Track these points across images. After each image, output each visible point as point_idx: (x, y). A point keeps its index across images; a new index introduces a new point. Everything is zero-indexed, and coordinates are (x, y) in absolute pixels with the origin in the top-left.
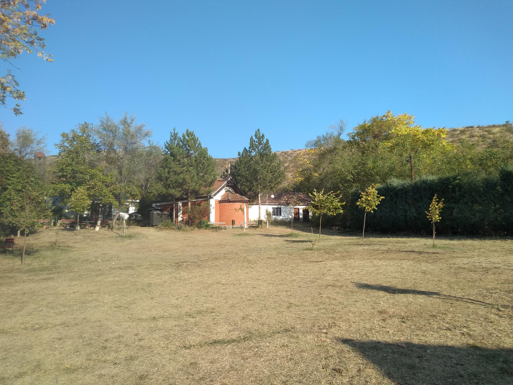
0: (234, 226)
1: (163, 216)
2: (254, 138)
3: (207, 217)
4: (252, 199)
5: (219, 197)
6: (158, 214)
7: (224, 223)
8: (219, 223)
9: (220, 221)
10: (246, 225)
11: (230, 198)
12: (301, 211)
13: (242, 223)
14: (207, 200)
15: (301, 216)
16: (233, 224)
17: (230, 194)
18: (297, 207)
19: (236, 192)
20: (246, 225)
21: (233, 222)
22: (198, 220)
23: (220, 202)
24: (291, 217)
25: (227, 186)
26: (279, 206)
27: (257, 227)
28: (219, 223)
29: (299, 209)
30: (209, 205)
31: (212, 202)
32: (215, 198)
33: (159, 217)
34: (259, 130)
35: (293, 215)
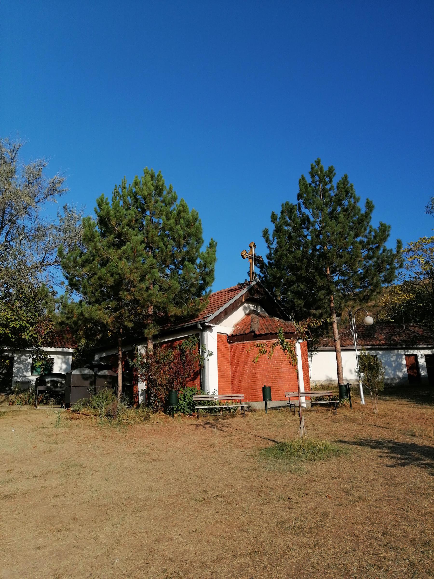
0: (270, 404)
1: (99, 381)
2: (309, 180)
3: (198, 381)
4: (318, 340)
5: (228, 326)
6: (85, 377)
7: (241, 396)
8: (230, 396)
9: (235, 391)
10: (303, 399)
11: (256, 328)
12: (422, 361)
13: (293, 394)
14: (197, 336)
15: (423, 373)
16: (265, 399)
17: (257, 319)
18: (411, 352)
19: (272, 313)
20: (303, 399)
21: (266, 394)
22: (175, 392)
23: (232, 339)
24: (401, 375)
25: (248, 301)
26: (373, 352)
27: (336, 406)
28: (230, 396)
29: (416, 356)
30: (201, 348)
31: (210, 340)
32: (217, 328)
33: (87, 383)
34: (318, 162)
35: (405, 370)
